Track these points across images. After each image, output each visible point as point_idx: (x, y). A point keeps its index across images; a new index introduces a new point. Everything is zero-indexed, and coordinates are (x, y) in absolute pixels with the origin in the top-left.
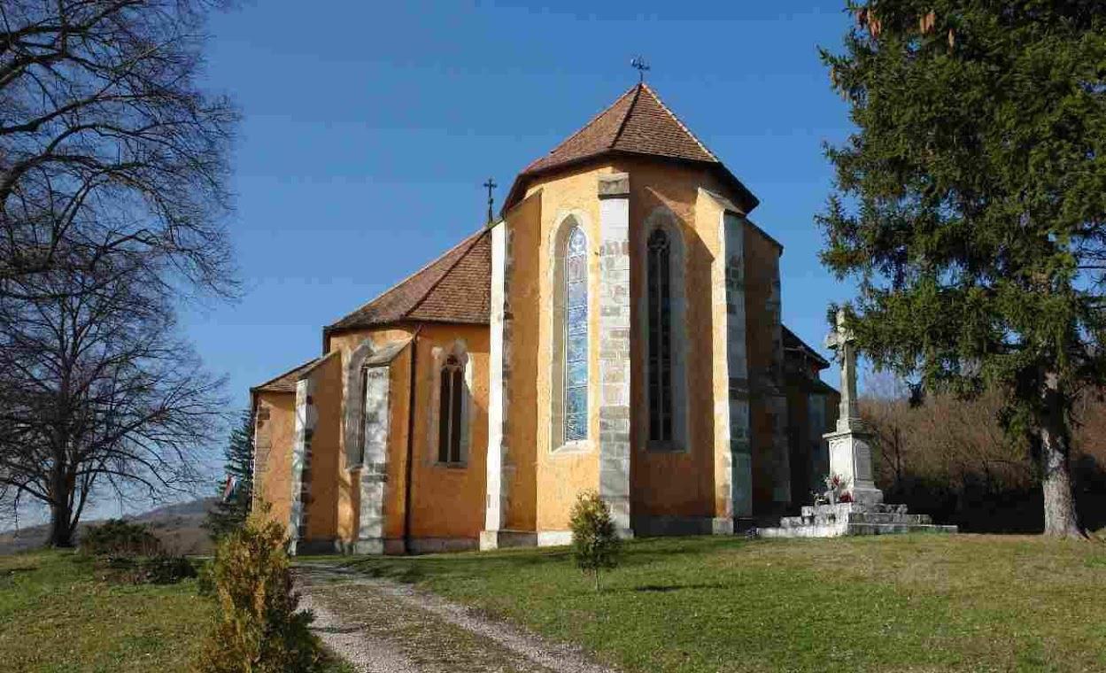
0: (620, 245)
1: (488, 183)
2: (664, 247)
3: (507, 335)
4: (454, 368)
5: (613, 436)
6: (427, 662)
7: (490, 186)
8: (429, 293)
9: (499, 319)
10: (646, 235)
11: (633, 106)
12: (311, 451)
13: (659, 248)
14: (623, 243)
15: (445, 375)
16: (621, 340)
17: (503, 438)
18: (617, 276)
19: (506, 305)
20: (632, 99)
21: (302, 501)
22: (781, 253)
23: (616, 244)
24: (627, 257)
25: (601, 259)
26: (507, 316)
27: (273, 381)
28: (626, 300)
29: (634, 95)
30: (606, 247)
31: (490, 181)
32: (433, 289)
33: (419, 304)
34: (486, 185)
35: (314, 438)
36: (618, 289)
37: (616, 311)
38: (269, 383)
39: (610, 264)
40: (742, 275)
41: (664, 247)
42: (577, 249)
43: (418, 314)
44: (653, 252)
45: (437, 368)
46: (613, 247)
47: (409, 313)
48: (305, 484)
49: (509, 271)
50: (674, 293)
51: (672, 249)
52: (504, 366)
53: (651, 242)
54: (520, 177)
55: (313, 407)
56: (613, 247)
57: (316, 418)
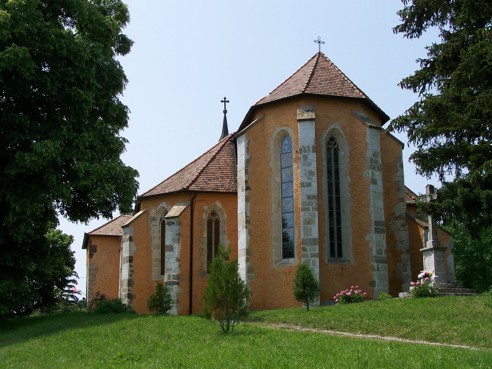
0: (311, 147)
1: (226, 100)
2: (335, 146)
3: (247, 200)
4: (214, 218)
5: (309, 255)
6: (448, 100)
7: (225, 101)
8: (198, 177)
9: (242, 191)
10: (325, 137)
11: (315, 67)
12: (133, 269)
13: (333, 147)
14: (313, 146)
15: (209, 222)
16: (312, 201)
17: (247, 258)
18: (309, 164)
19: (246, 182)
20: (315, 62)
21: (128, 298)
22: (403, 149)
23: (308, 147)
24: (315, 154)
25: (300, 156)
26: (247, 188)
27: (97, 229)
28: (315, 178)
29: (316, 60)
30: (303, 149)
31: (225, 98)
32: (200, 174)
33: (193, 182)
34: (222, 101)
35: (134, 262)
36: (311, 173)
37: (309, 185)
38: (95, 230)
39: (305, 158)
40: (380, 162)
41: (335, 146)
42: (286, 149)
43: (192, 188)
44: (328, 149)
45: (205, 217)
46: (307, 149)
47: (188, 187)
48: (130, 288)
49: (247, 162)
50: (341, 174)
51: (340, 147)
52: (246, 217)
53: (328, 144)
54: (251, 107)
55: (133, 243)
56: (307, 149)
57: (134, 248)
